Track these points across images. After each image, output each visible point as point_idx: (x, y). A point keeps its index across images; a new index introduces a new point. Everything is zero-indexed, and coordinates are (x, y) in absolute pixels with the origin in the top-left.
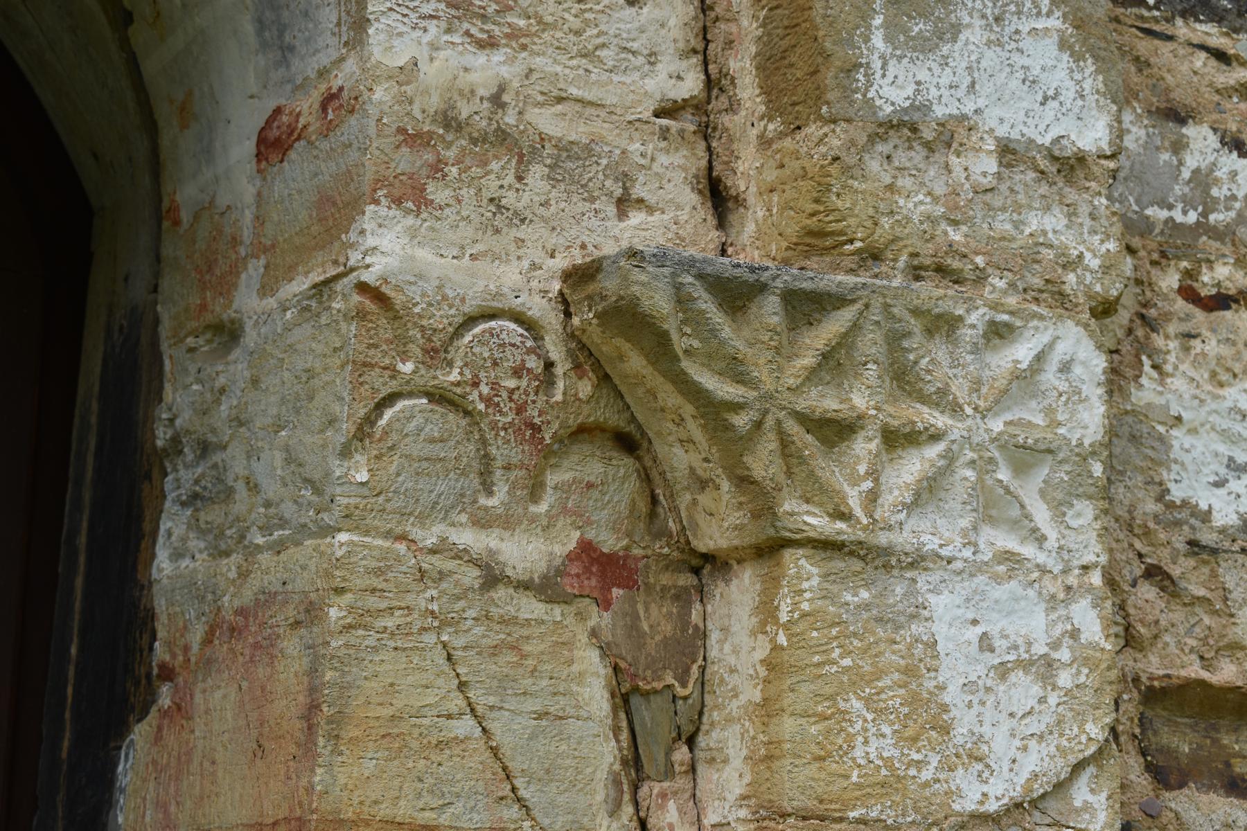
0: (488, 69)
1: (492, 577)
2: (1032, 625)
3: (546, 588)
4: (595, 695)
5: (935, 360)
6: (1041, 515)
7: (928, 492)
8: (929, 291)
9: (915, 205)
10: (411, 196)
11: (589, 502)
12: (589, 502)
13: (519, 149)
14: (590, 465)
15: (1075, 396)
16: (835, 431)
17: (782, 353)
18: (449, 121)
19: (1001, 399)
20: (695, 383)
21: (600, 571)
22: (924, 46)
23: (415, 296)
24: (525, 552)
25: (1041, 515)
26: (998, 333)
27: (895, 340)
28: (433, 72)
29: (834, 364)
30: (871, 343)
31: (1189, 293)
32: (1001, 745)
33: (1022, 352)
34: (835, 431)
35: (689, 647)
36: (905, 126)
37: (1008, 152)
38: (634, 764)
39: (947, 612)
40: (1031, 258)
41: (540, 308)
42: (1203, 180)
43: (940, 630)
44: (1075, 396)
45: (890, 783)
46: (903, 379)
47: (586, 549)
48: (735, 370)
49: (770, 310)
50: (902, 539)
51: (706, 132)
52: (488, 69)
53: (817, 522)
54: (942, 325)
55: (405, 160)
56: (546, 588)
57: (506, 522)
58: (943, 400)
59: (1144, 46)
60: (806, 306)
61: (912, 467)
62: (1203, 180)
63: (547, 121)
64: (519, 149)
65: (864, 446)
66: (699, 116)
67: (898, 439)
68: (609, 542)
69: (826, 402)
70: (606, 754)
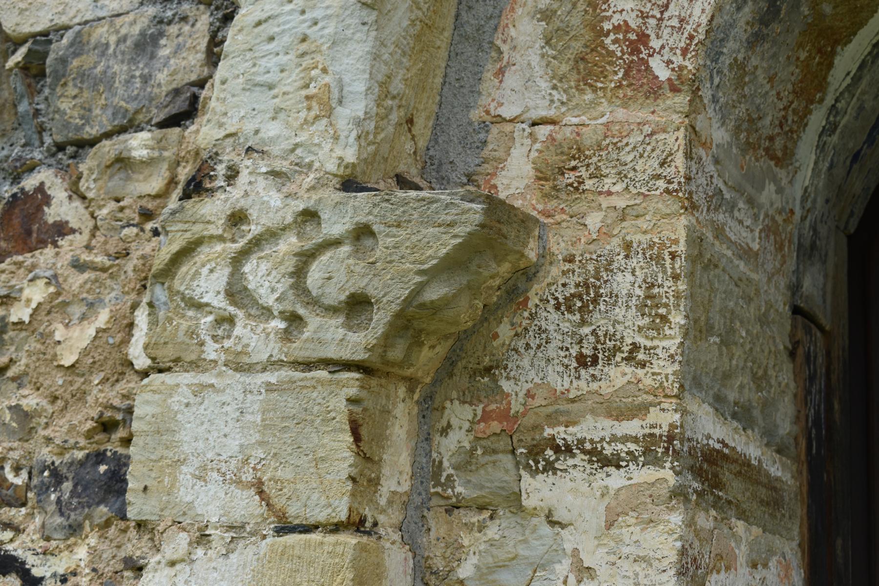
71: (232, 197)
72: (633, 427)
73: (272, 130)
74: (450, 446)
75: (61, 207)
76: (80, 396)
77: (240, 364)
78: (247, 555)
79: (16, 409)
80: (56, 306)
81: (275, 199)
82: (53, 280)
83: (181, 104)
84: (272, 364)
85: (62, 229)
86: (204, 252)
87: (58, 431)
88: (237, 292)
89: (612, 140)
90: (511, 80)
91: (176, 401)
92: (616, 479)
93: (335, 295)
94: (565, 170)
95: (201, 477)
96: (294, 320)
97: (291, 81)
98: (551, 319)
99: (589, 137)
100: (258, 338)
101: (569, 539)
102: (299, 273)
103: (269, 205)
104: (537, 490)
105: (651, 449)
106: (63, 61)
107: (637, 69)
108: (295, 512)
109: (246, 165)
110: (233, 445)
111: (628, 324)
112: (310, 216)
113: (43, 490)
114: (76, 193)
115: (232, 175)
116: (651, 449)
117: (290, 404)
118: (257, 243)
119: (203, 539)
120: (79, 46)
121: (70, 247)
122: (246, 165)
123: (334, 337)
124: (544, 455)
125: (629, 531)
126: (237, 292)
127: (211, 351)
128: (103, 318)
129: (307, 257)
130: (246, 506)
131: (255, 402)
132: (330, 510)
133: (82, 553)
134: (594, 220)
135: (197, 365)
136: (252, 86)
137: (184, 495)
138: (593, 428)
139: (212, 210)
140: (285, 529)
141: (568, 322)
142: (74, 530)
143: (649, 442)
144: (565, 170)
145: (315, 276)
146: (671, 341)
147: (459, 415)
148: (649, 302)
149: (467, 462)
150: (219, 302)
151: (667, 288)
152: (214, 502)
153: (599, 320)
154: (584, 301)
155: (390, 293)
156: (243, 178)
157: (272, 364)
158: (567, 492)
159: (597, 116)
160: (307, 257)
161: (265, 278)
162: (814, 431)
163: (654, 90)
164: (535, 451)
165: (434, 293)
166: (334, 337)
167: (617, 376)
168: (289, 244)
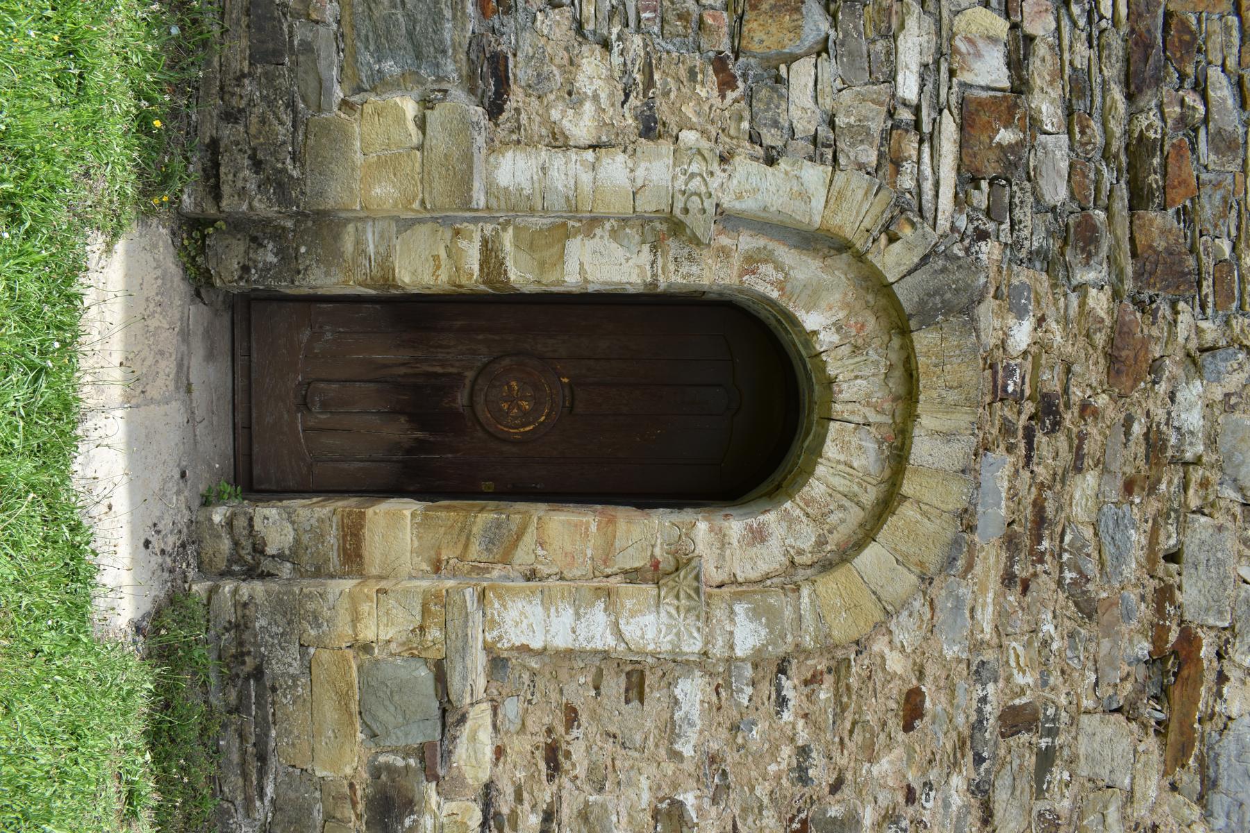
0: (735, 542)
1: (653, 546)
2: (650, 635)
3: (652, 556)
4: (636, 565)
5: (693, 614)
6: (668, 638)
7: (670, 615)
8: (703, 615)
9: (718, 613)
10: (711, 530)
11: (667, 564)
12: (667, 564)
13: (723, 546)
14: (673, 563)
15: (690, 646)
16: (677, 597)
17: (689, 586)
18: (724, 535)
19: (687, 630)
20: (481, 270)
21: (656, 565)
22: (747, 615)
23: (695, 531)
24: (657, 552)
25: (668, 638)
26: (698, 629)
27: (694, 608)
28: (732, 532)
29: (689, 596)
30: (693, 603)
31: (718, 686)
32: (630, 628)
33: (696, 634)
34: (677, 597)
35: (645, 581)
36: (732, 612)
37: (732, 633)
38: (625, 572)
39: (650, 618)
40: (713, 637)
41: (697, 552)
42: (742, 691)
43: (647, 617)
44: (690, 646)
45: (623, 606)
46: (688, 610)
47: (659, 562)
48: (685, 578)
49: (695, 584)
50: (661, 610)
51: (732, 583)
52: (735, 542)
53: (663, 594)
54: (698, 618)
55: (717, 529)
56: (652, 556)
57: (662, 548)
58: (685, 618)
59: (768, 679)
60: (697, 591)
61: (674, 612)
62: (742, 691)
63: (728, 553)
64: (723, 546)
65: (676, 602)
66: (735, 582)
67: (678, 608)
68: (661, 566)
69: (682, 595)
70: (627, 567)
71: (718, 172)
72: (660, 271)
73: (735, 181)
74: (657, 225)
75: (731, 95)
76: (673, 113)
77: (674, 178)
78: (628, 183)
79: (670, 90)
80: (700, 102)
81: (715, 185)
82: (708, 99)
83: (755, 138)
84: (673, 187)
85: (723, 97)
86: (704, 164)
87: (664, 108)
88: (693, 175)
89: (730, 265)
90: (749, 239)
91: (666, 159)
92: (648, 267)
93: (689, 205)
94: (724, 253)
95: (647, 169)
96: (684, 192)
97: (748, 187)
98: (687, 250)
99: (731, 260)
100: (680, 184)
101: (634, 256)
102: (695, 194)
103: (714, 184)
104: (646, 248)
105: (655, 275)
106: (777, 91)
107: (747, 272)
108: (638, 196)
109: (726, 175)
110: (654, 178)
111: (684, 270)
112: (710, 195)
113: (647, 104)
114: (736, 101)
115: (724, 171)
116: (655, 275)
117: (663, 193)
118: (704, 180)
119: (632, 171)
120: (781, 96)
121: (717, 101)
122: (726, 175)
123: (679, 206)
124: (654, 249)
125: (637, 271)
126: (693, 175)
127: (678, 169)
128: (694, 120)
129: (699, 195)
130: (639, 183)
131: (664, 183)
132: (537, 753)
133: (630, 121)
134: (710, 261)
135: (674, 165)
136: (748, 174)
137: (642, 164)
138: (660, 261)
139: (715, 166)
140: (634, 194)
141: (686, 254)
142: (636, 118)
143: (656, 275)
144: (724, 253)
145: (695, 198)
146: (679, 280)
147: (664, 227)
148: (689, 275)
149: (653, 229)
150: (690, 171)
151: (692, 279)
152: (640, 173)
153: (686, 262)
154: (690, 258)
155: (687, 220)
156: (723, 174)
157: (673, 187)
158: (646, 255)
159: (736, 261)
160: (699, 195)
161: (696, 184)
162: (270, 814)
163: (741, 276)
164: (655, 247)
165: (688, 231)
166: (679, 206)
167: (672, 267)
168: (703, 189)
